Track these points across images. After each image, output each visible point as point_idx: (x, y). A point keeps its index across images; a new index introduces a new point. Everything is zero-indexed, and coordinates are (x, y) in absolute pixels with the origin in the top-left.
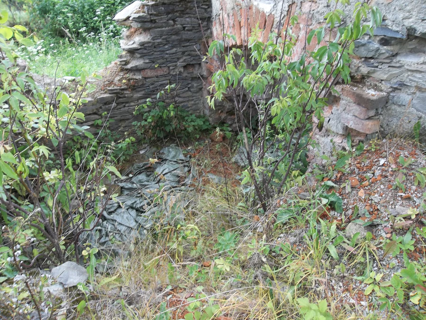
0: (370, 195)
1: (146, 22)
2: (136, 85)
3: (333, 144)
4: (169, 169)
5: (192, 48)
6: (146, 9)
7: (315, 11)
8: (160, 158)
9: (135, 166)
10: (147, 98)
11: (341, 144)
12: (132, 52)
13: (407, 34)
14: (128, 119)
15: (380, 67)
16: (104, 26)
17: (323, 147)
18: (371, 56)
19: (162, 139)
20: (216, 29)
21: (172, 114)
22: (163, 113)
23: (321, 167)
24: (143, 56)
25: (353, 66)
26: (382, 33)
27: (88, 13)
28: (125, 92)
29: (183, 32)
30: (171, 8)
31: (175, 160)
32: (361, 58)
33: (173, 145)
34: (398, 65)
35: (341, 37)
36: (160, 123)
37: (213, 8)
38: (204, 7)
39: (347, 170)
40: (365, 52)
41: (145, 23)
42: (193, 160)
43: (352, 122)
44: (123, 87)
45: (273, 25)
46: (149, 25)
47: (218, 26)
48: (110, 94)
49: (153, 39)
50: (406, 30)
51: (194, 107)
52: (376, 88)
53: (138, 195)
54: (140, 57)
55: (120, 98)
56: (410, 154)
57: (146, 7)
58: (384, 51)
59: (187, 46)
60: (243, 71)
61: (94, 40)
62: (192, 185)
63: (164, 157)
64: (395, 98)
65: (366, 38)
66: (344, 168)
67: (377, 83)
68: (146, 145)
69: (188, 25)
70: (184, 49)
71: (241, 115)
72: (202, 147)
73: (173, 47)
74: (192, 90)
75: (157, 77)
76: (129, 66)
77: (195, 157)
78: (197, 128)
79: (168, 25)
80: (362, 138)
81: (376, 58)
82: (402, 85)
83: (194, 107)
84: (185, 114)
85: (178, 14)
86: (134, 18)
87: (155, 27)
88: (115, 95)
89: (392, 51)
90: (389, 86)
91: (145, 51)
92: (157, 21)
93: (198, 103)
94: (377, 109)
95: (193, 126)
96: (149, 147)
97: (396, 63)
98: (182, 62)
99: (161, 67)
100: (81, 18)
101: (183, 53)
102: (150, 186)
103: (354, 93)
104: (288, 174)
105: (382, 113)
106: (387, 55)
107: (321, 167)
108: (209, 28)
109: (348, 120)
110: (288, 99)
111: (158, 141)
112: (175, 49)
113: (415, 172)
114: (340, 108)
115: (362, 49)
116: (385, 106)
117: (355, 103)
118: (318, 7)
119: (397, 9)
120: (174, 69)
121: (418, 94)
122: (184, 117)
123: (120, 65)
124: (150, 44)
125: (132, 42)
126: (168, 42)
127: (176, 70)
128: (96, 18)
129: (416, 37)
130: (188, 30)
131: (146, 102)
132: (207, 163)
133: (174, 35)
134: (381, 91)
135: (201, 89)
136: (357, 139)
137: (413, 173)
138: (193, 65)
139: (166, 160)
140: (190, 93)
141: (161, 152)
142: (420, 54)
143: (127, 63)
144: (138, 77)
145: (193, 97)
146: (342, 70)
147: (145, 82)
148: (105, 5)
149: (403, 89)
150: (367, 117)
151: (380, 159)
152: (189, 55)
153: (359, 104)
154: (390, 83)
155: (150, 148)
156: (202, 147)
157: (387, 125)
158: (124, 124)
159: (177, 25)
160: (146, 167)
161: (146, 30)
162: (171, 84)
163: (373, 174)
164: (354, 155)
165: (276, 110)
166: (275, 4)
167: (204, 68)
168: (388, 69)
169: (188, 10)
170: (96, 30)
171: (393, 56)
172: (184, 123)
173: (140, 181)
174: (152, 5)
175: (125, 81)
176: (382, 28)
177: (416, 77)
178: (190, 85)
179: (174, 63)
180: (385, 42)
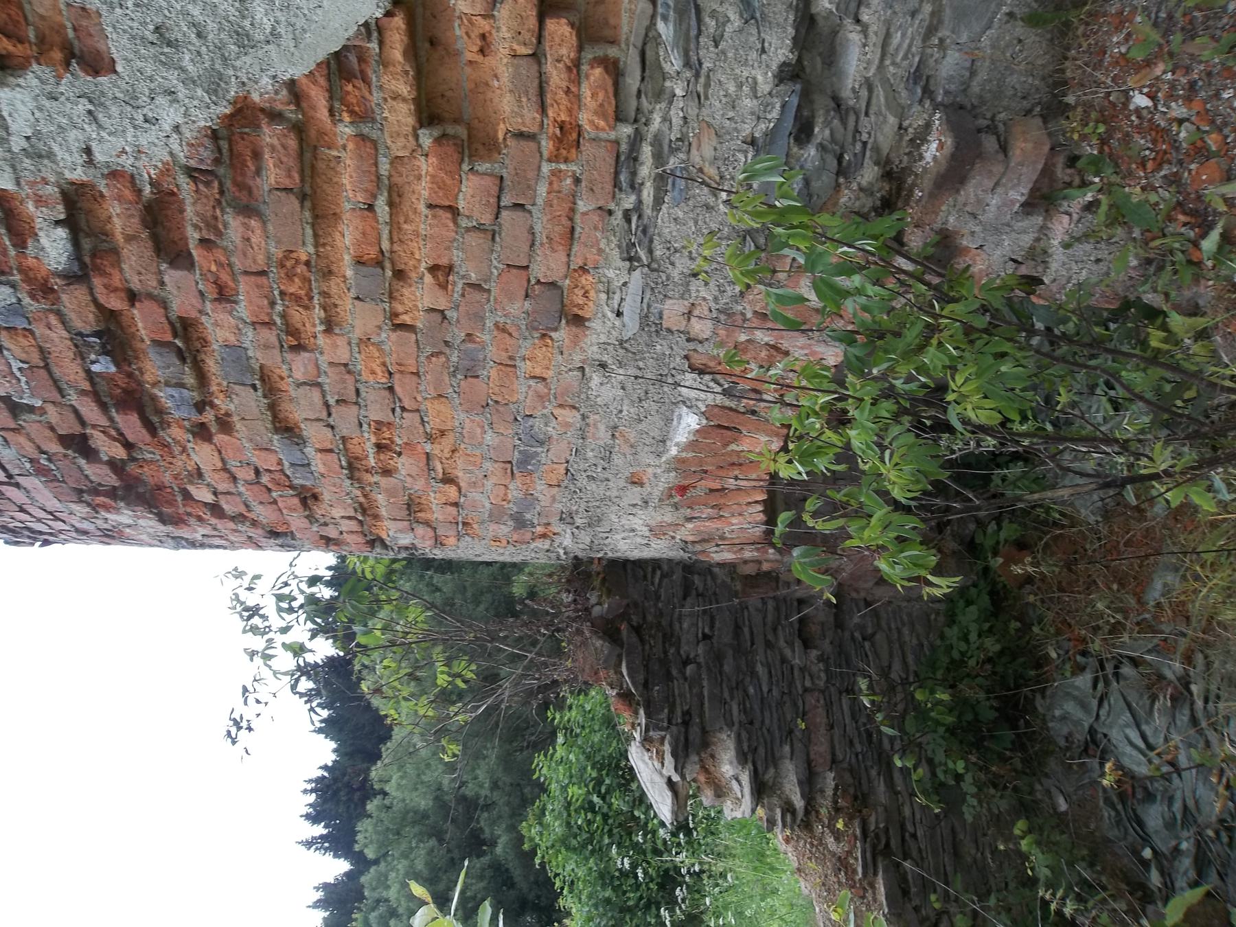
1: (687, 739)
2: (852, 790)
3: (1078, 240)
4: (1127, 726)
7: (713, 305)
8: (1086, 750)
9: (1113, 834)
10: (890, 764)
11: (1075, 216)
12: (761, 790)
13: (790, 83)
14: (953, 830)
15: (865, 137)
16: (660, 853)
17: (1076, 261)
18: (835, 162)
19: (1018, 735)
21: (944, 696)
22: (938, 723)
23: (1152, 269)
24: (773, 760)
25: (857, 204)
26: (783, 142)
27: (625, 893)
28: (872, 828)
29: (715, 640)
31: (1095, 703)
32: (838, 185)
33: (1039, 702)
34: (864, 93)
36: (969, 734)
37: (664, 556)
38: (657, 581)
39: (1164, 196)
40: (824, 178)
41: (690, 745)
42: (1096, 646)
43: (1011, 193)
44: (858, 832)
45: (731, 409)
46: (695, 731)
48: (875, 874)
49: (730, 725)
50: (782, 87)
52: (921, 137)
53: (1225, 839)
54: (776, 766)
55: (887, 845)
56: (1118, 29)
57: (651, 733)
58: (827, 132)
59: (752, 633)
60: (868, 496)
61: (696, 891)
62: (1188, 659)
63: (1080, 737)
64: (953, 87)
66: (1157, 204)
68: (1038, 787)
69: (700, 624)
70: (759, 641)
71: (972, 501)
72: (1050, 615)
73: (753, 674)
74: (870, 631)
75: (832, 727)
76: (799, 803)
77: (1084, 640)
78: (986, 626)
79: (695, 681)
80: (1060, 160)
81: (842, 147)
82: (921, 78)
84: (945, 660)
85: (672, 651)
86: (676, 769)
87: (702, 715)
88: (880, 859)
89: (828, 112)
90: (916, 108)
91: (761, 751)
92: (686, 708)
93: (910, 615)
94: (979, 131)
95: (980, 636)
96: (1044, 780)
97: (858, 98)
98: (793, 651)
100: (635, 915)
101: (769, 645)
102: (1188, 794)
103: (932, 196)
104: (1154, 359)
105: (989, 115)
106: (836, 122)
107: (1152, 269)
108: (708, 570)
109: (1004, 205)
110: (957, 377)
111: (1023, 748)
112: (760, 669)
113: (1181, 10)
115: (816, 185)
116: (970, 112)
117: (958, 191)
118: (704, 299)
119: (731, 114)
120: (811, 676)
121: (944, 32)
122: (953, 661)
123: (792, 829)
124: (744, 735)
125: (735, 784)
126: (740, 685)
127: (815, 669)
128: (640, 872)
129: (799, 60)
130: (712, 627)
131: (905, 771)
132: (1106, 602)
133: (721, 666)
136: (1062, 173)
137: (1184, 15)
139: (1092, 731)
140: (878, 637)
141: (1062, 743)
142: (838, 41)
143: (789, 809)
144: (829, 780)
145: (890, 629)
146: (882, 239)
147: (845, 765)
148: (606, 841)
149: (927, 72)
150: (1001, 156)
151: (1132, 107)
152: (775, 630)
153: (963, 180)
154: (910, 106)
155: (1047, 776)
156: (1050, 615)
157: (1024, 98)
158: (969, 849)
160: (1115, 799)
161: (705, 744)
162: (851, 690)
163: (1181, 122)
164: (1115, 179)
166: (684, 402)
168: (873, 118)
169: (664, 623)
170: (669, 879)
171: (839, 106)
172: (972, 662)
173: (1170, 825)
174: (648, 715)
175: (840, 820)
177: (899, 46)
178: (857, 635)
179: (796, 672)
180: (803, 132)
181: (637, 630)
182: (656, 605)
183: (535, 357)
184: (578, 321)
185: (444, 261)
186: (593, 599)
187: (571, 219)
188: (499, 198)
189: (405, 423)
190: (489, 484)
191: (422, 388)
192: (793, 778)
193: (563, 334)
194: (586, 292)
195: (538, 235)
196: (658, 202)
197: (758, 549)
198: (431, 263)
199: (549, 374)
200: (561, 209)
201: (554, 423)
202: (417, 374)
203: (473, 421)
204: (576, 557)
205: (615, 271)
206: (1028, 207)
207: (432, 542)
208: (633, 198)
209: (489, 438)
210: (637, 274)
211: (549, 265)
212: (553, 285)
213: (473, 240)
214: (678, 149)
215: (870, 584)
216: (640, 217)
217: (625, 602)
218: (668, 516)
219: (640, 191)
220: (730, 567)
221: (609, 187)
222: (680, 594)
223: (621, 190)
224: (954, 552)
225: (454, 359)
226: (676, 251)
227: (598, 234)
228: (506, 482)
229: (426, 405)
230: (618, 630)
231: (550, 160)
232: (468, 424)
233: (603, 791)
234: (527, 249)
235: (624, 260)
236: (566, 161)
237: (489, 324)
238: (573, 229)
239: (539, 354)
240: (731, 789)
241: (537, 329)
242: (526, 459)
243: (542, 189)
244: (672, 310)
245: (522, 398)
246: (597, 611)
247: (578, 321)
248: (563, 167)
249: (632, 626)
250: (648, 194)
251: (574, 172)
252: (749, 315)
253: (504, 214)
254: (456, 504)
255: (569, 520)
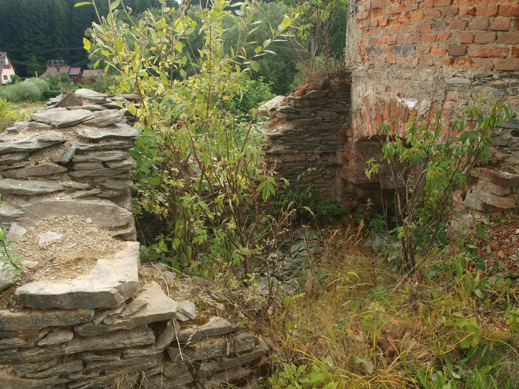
0: (508, 255)
1: (291, 113)
5: (329, 138)
6: (292, 102)
15: (513, 153)
17: (461, 223)
20: (355, 123)
26: (513, 126)
29: (322, 123)
30: (314, 102)
32: (496, 146)
35: (480, 125)
38: (343, 102)
41: (289, 114)
46: (293, 116)
47: (358, 119)
49: (295, 128)
51: (325, 193)
52: (510, 171)
58: (516, 141)
59: (325, 136)
65: (500, 130)
67: (511, 167)
70: (323, 138)
76: (271, 151)
79: (309, 116)
83: (325, 193)
85: (320, 108)
86: (282, 109)
91: (287, 138)
92: (301, 113)
94: (511, 189)
99: (299, 153)
101: (321, 142)
103: (491, 174)
112: (314, 138)
114: (479, 187)
115: (497, 139)
117: (492, 182)
118: (458, 105)
124: (292, 133)
125: (275, 130)
126: (308, 131)
127: (313, 157)
130: (327, 122)
133: (314, 125)
134: (515, 173)
135: (333, 177)
138: (328, 154)
140: (323, 179)
143: (269, 148)
150: (503, 194)
152: (326, 144)
153: (495, 183)
159: (318, 117)
163: (511, 240)
165: (430, 176)
167: (339, 157)
176: (513, 123)
181: (326, 95)
182: (334, 102)
183: (438, 48)
184: (452, 62)
185: (477, 13)
186: (336, 80)
187: (490, 57)
188: (500, 31)
189: (413, 4)
190: (387, 37)
191: (427, 9)
192: (279, 149)
193: (447, 57)
194: (463, 64)
195: (485, 45)
196: (495, 86)
197: (358, 135)
198: (477, 8)
199: (432, 54)
200: (494, 53)
201: (412, 57)
202: (433, 7)
203: (414, 28)
204: (351, 73)
205: (470, 73)
206: (485, 205)
207: (360, 18)
208: (497, 77)
209: (407, 35)
210: (469, 81)
211: (474, 50)
212: (466, 52)
213: (485, 23)
214: (514, 91)
215: (342, 176)
216: (490, 80)
217: (336, 91)
218: (372, 102)
219: (499, 80)
220: (349, 126)
221: (502, 69)
222: (338, 111)
223: (500, 73)
224: (352, 204)
225: (439, 20)
226: (476, 94)
227: (484, 66)
228: (388, 43)
229: (420, 11)
230: (326, 89)
231: (513, 47)
232: (412, 27)
233: (236, 99)
234: (481, 41)
235: (474, 76)
236: (512, 53)
237: (452, 31)
238: (487, 57)
239: (440, 50)
240: (273, 129)
241: (449, 48)
242: (398, 49)
243: (502, 46)
244: (452, 95)
245: (423, 45)
246: (332, 81)
247: (452, 62)
248: (510, 52)
249: (327, 94)
250: (498, 82)
251: (508, 56)
252: (451, 120)
253: (494, 33)
254: (378, 26)
255: (371, 67)
